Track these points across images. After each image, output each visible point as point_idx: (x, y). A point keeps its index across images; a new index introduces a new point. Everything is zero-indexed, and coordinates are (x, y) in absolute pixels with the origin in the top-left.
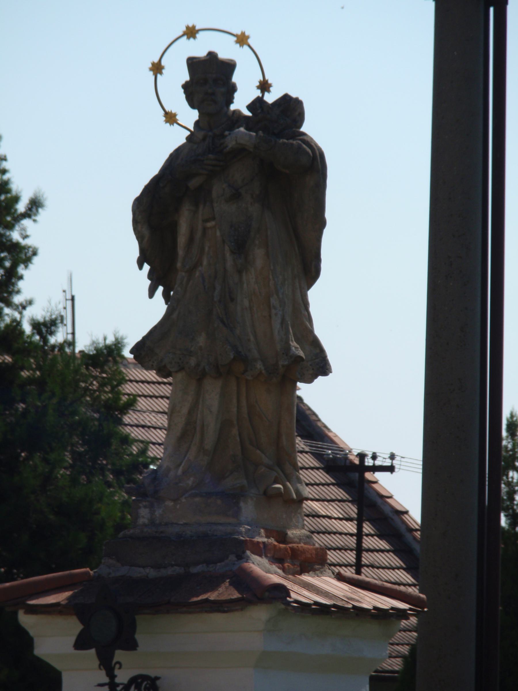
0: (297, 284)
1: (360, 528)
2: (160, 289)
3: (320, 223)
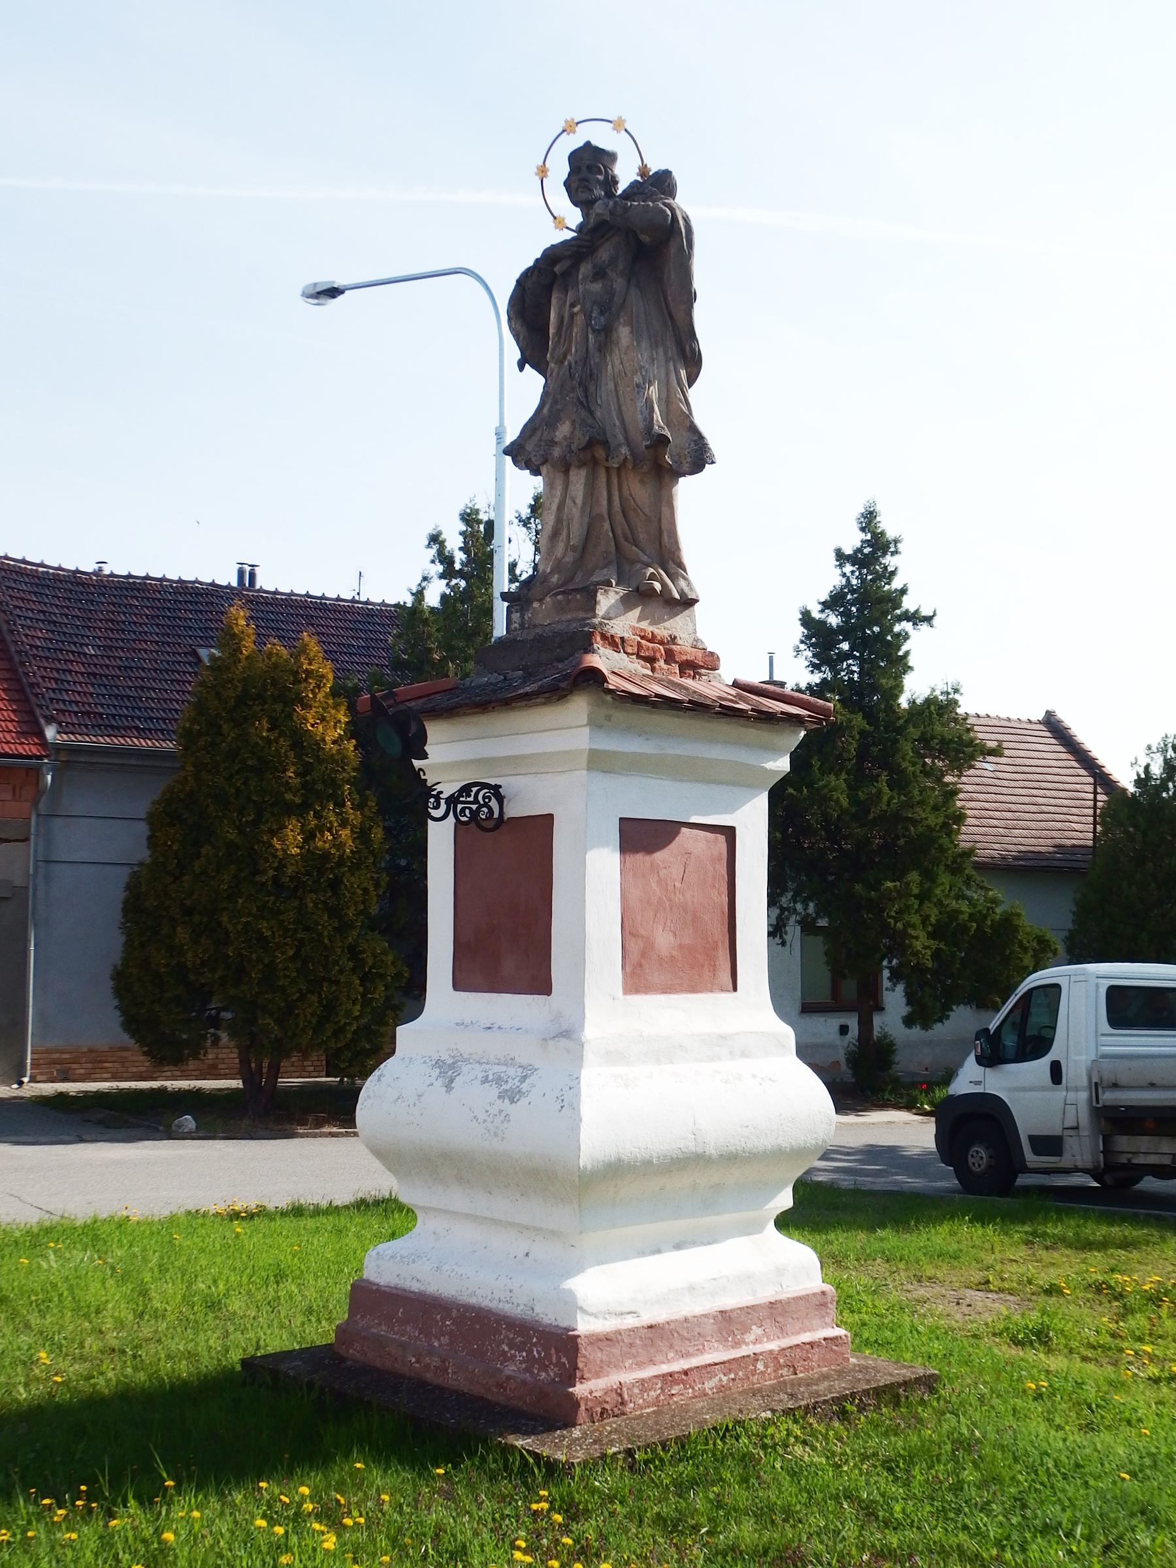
0: (672, 368)
1: (1095, 789)
2: (901, 653)
3: (690, 298)
